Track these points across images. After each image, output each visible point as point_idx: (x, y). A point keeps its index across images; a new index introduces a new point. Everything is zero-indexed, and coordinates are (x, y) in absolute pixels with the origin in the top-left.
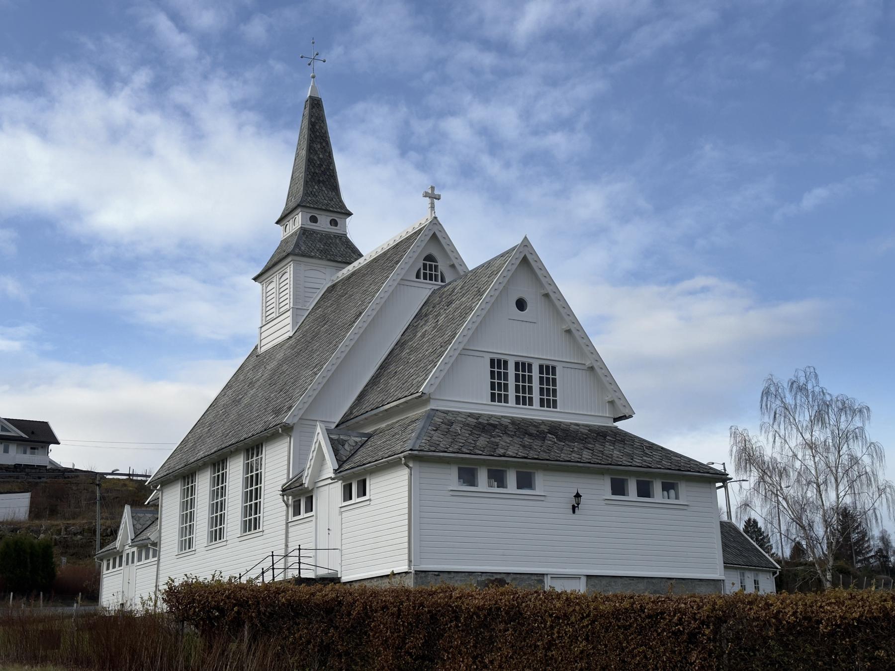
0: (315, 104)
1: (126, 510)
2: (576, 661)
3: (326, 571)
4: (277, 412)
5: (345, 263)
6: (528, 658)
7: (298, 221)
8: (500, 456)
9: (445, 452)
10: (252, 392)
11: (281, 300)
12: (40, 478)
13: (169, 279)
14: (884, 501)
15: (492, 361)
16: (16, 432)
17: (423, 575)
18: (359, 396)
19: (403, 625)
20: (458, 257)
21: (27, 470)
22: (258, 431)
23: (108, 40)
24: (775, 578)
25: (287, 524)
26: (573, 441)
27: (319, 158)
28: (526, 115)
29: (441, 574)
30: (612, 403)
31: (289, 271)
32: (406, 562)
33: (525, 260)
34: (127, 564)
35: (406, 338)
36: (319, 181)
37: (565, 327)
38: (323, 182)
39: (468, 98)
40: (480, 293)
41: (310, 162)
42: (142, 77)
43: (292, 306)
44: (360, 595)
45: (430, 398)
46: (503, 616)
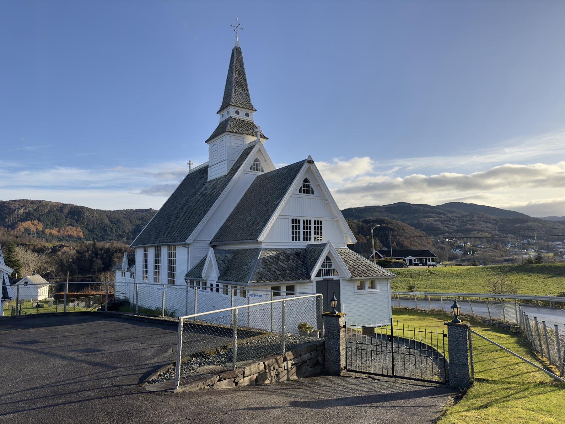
0: (237, 53)
11: (221, 152)
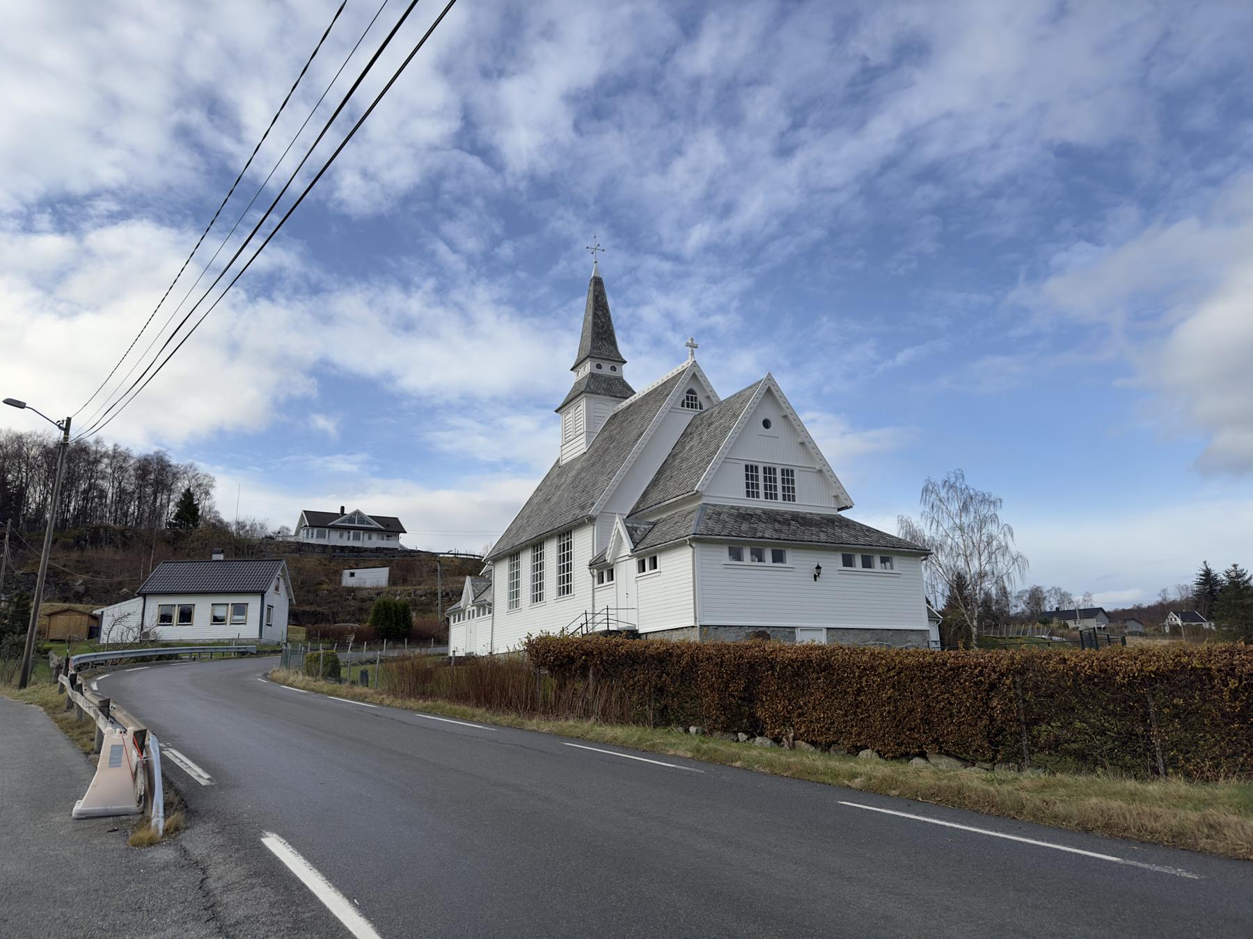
0: (598, 282)
1: (467, 580)
2: (884, 705)
3: (626, 625)
4: (583, 508)
5: (622, 398)
6: (839, 702)
7: (587, 368)
8: (760, 538)
9: (719, 535)
10: (559, 493)
11: (577, 430)
12: (393, 557)
13: (456, 421)
14: (1017, 567)
15: (747, 466)
16: (376, 525)
17: (706, 628)
18: (643, 495)
19: (727, 673)
20: (712, 391)
21: (385, 552)
22: (569, 521)
23: (405, 259)
24: (939, 626)
25: (593, 590)
26: (811, 525)
27: (601, 321)
28: (697, 302)
29: (719, 628)
30: (836, 497)
31: (583, 404)
32: (693, 618)
33: (769, 390)
34: (469, 618)
35: (676, 450)
36: (602, 339)
37: (800, 440)
38: (605, 339)
39: (654, 293)
40: (735, 416)
41: (595, 324)
42: (430, 283)
43: (585, 429)
44: (688, 648)
45: (702, 495)
46: (814, 668)
